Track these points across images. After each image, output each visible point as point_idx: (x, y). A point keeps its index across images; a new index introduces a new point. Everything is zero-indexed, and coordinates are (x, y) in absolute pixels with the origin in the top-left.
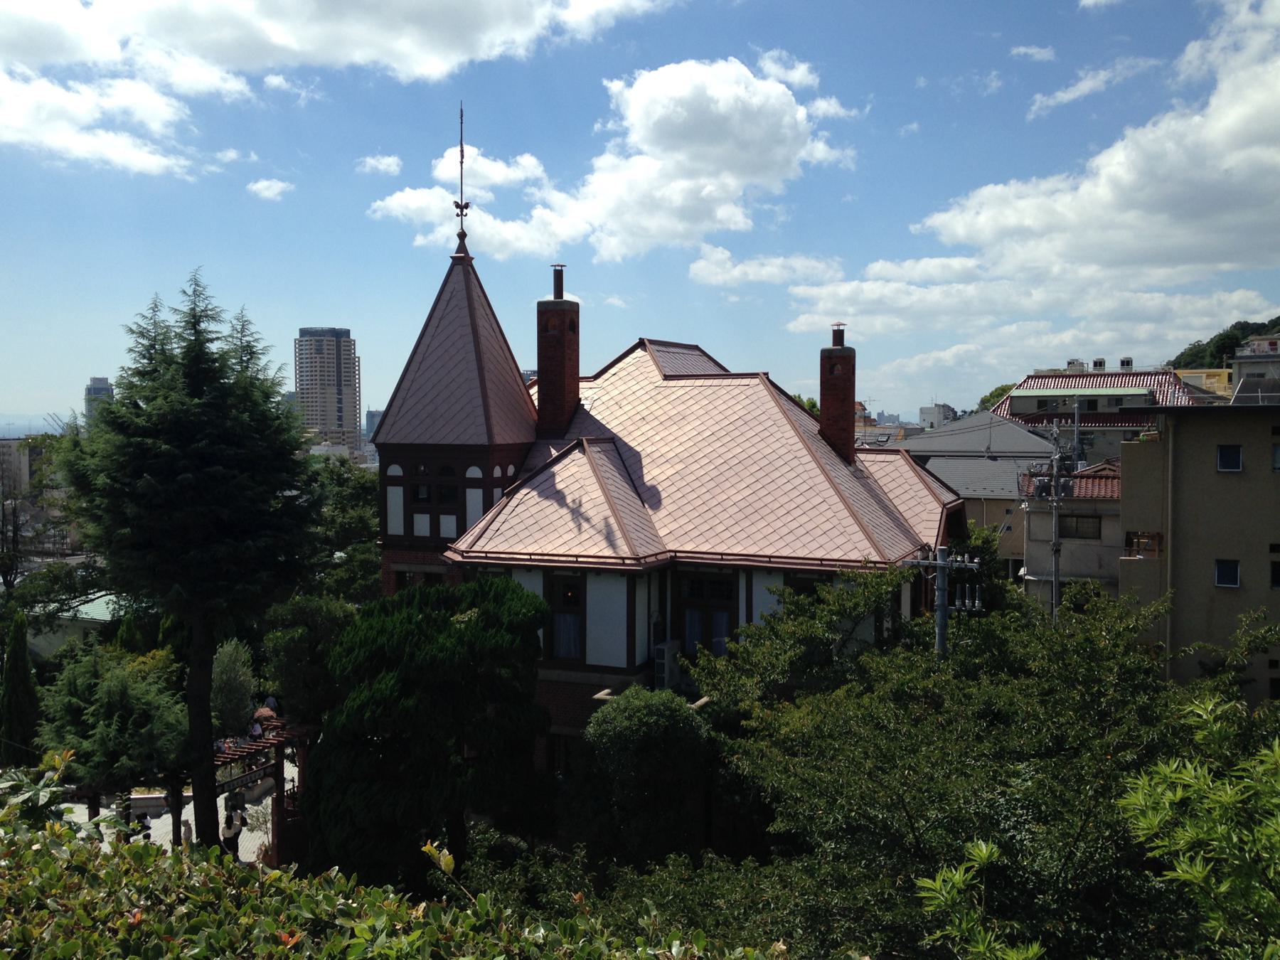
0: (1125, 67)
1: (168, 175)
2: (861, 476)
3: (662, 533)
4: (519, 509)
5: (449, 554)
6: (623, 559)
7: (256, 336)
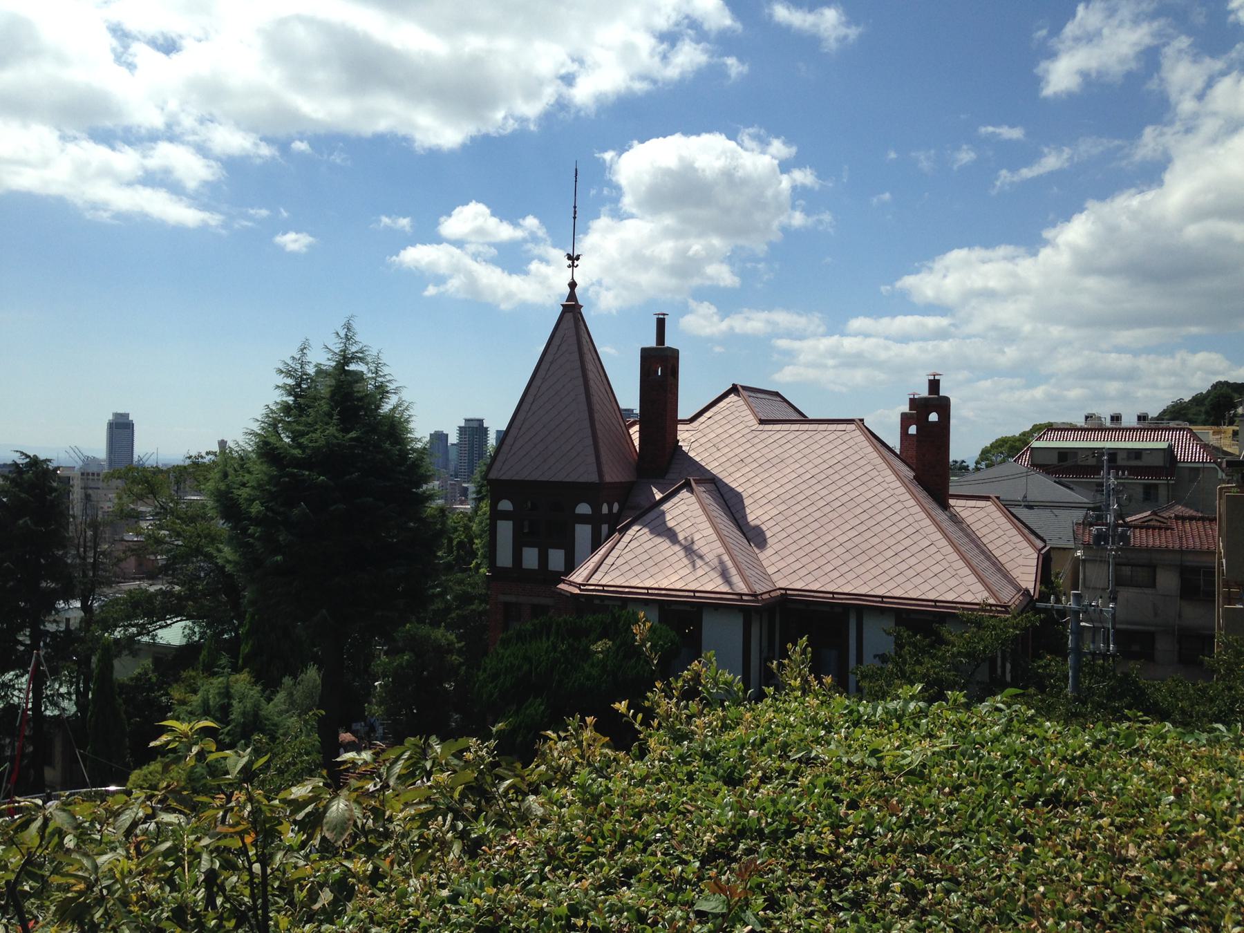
0: (1089, 147)
1: (204, 228)
2: (956, 520)
3: (770, 570)
4: (632, 545)
5: (561, 586)
6: (741, 595)
7: (388, 378)
